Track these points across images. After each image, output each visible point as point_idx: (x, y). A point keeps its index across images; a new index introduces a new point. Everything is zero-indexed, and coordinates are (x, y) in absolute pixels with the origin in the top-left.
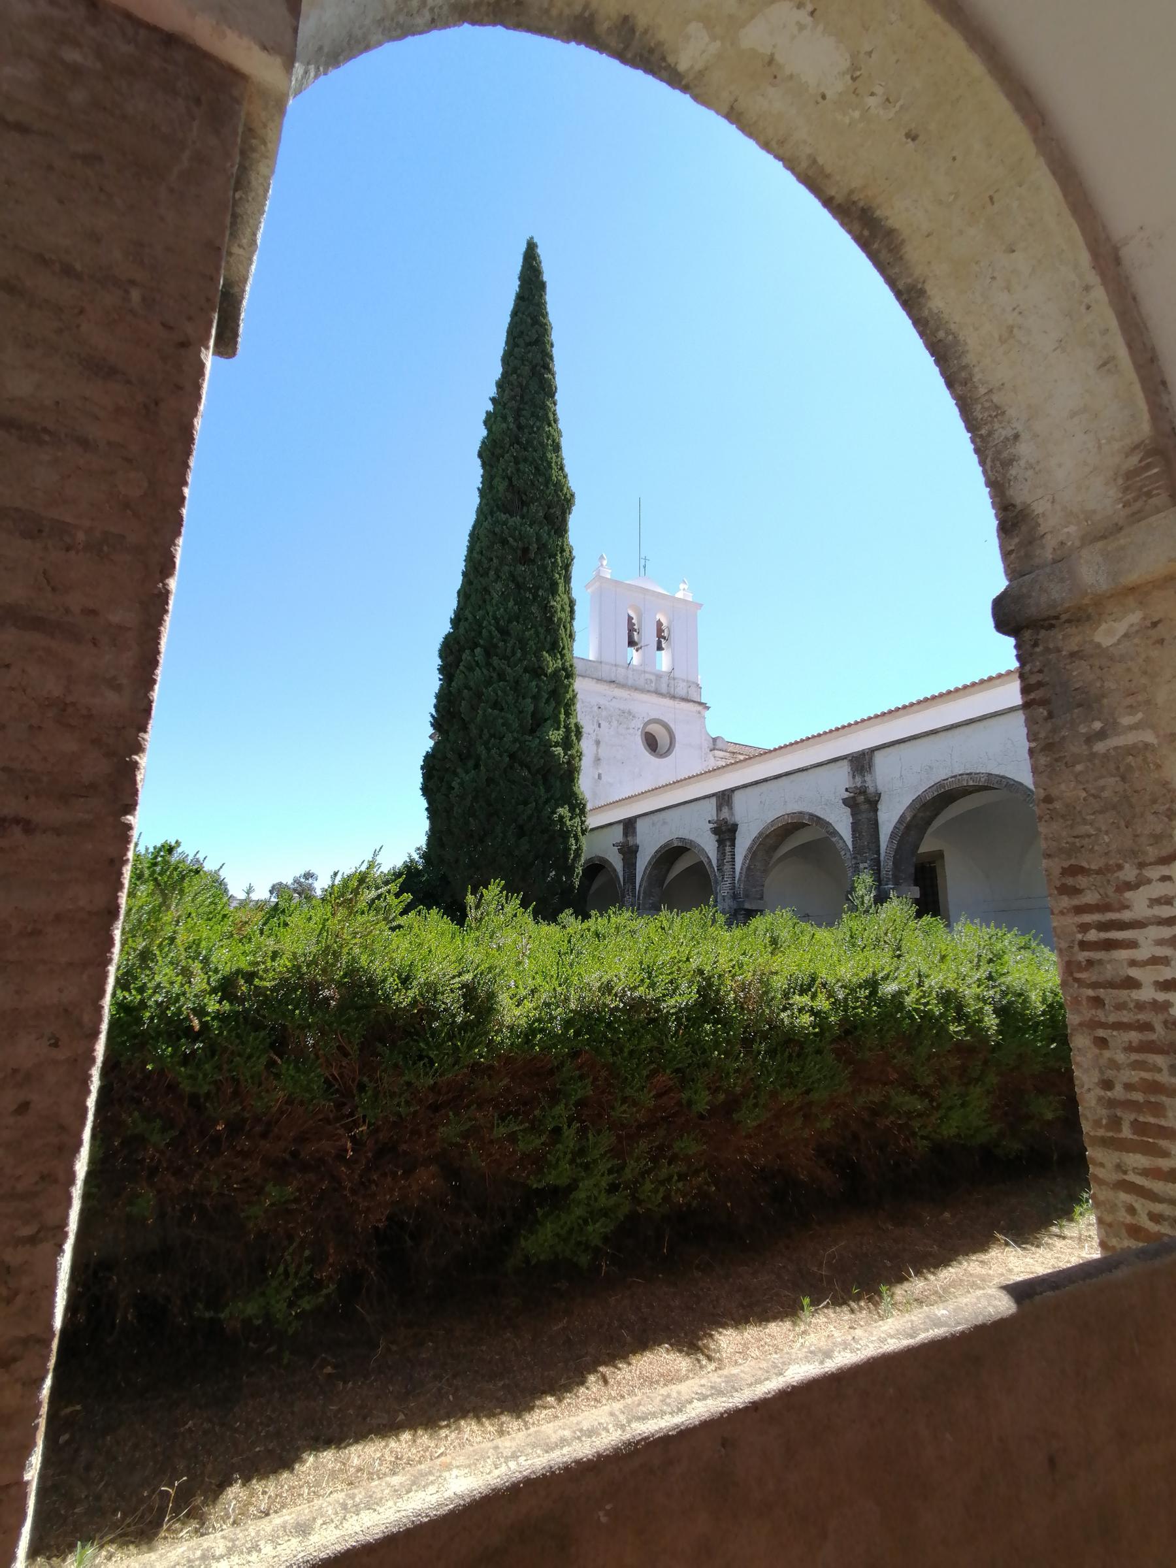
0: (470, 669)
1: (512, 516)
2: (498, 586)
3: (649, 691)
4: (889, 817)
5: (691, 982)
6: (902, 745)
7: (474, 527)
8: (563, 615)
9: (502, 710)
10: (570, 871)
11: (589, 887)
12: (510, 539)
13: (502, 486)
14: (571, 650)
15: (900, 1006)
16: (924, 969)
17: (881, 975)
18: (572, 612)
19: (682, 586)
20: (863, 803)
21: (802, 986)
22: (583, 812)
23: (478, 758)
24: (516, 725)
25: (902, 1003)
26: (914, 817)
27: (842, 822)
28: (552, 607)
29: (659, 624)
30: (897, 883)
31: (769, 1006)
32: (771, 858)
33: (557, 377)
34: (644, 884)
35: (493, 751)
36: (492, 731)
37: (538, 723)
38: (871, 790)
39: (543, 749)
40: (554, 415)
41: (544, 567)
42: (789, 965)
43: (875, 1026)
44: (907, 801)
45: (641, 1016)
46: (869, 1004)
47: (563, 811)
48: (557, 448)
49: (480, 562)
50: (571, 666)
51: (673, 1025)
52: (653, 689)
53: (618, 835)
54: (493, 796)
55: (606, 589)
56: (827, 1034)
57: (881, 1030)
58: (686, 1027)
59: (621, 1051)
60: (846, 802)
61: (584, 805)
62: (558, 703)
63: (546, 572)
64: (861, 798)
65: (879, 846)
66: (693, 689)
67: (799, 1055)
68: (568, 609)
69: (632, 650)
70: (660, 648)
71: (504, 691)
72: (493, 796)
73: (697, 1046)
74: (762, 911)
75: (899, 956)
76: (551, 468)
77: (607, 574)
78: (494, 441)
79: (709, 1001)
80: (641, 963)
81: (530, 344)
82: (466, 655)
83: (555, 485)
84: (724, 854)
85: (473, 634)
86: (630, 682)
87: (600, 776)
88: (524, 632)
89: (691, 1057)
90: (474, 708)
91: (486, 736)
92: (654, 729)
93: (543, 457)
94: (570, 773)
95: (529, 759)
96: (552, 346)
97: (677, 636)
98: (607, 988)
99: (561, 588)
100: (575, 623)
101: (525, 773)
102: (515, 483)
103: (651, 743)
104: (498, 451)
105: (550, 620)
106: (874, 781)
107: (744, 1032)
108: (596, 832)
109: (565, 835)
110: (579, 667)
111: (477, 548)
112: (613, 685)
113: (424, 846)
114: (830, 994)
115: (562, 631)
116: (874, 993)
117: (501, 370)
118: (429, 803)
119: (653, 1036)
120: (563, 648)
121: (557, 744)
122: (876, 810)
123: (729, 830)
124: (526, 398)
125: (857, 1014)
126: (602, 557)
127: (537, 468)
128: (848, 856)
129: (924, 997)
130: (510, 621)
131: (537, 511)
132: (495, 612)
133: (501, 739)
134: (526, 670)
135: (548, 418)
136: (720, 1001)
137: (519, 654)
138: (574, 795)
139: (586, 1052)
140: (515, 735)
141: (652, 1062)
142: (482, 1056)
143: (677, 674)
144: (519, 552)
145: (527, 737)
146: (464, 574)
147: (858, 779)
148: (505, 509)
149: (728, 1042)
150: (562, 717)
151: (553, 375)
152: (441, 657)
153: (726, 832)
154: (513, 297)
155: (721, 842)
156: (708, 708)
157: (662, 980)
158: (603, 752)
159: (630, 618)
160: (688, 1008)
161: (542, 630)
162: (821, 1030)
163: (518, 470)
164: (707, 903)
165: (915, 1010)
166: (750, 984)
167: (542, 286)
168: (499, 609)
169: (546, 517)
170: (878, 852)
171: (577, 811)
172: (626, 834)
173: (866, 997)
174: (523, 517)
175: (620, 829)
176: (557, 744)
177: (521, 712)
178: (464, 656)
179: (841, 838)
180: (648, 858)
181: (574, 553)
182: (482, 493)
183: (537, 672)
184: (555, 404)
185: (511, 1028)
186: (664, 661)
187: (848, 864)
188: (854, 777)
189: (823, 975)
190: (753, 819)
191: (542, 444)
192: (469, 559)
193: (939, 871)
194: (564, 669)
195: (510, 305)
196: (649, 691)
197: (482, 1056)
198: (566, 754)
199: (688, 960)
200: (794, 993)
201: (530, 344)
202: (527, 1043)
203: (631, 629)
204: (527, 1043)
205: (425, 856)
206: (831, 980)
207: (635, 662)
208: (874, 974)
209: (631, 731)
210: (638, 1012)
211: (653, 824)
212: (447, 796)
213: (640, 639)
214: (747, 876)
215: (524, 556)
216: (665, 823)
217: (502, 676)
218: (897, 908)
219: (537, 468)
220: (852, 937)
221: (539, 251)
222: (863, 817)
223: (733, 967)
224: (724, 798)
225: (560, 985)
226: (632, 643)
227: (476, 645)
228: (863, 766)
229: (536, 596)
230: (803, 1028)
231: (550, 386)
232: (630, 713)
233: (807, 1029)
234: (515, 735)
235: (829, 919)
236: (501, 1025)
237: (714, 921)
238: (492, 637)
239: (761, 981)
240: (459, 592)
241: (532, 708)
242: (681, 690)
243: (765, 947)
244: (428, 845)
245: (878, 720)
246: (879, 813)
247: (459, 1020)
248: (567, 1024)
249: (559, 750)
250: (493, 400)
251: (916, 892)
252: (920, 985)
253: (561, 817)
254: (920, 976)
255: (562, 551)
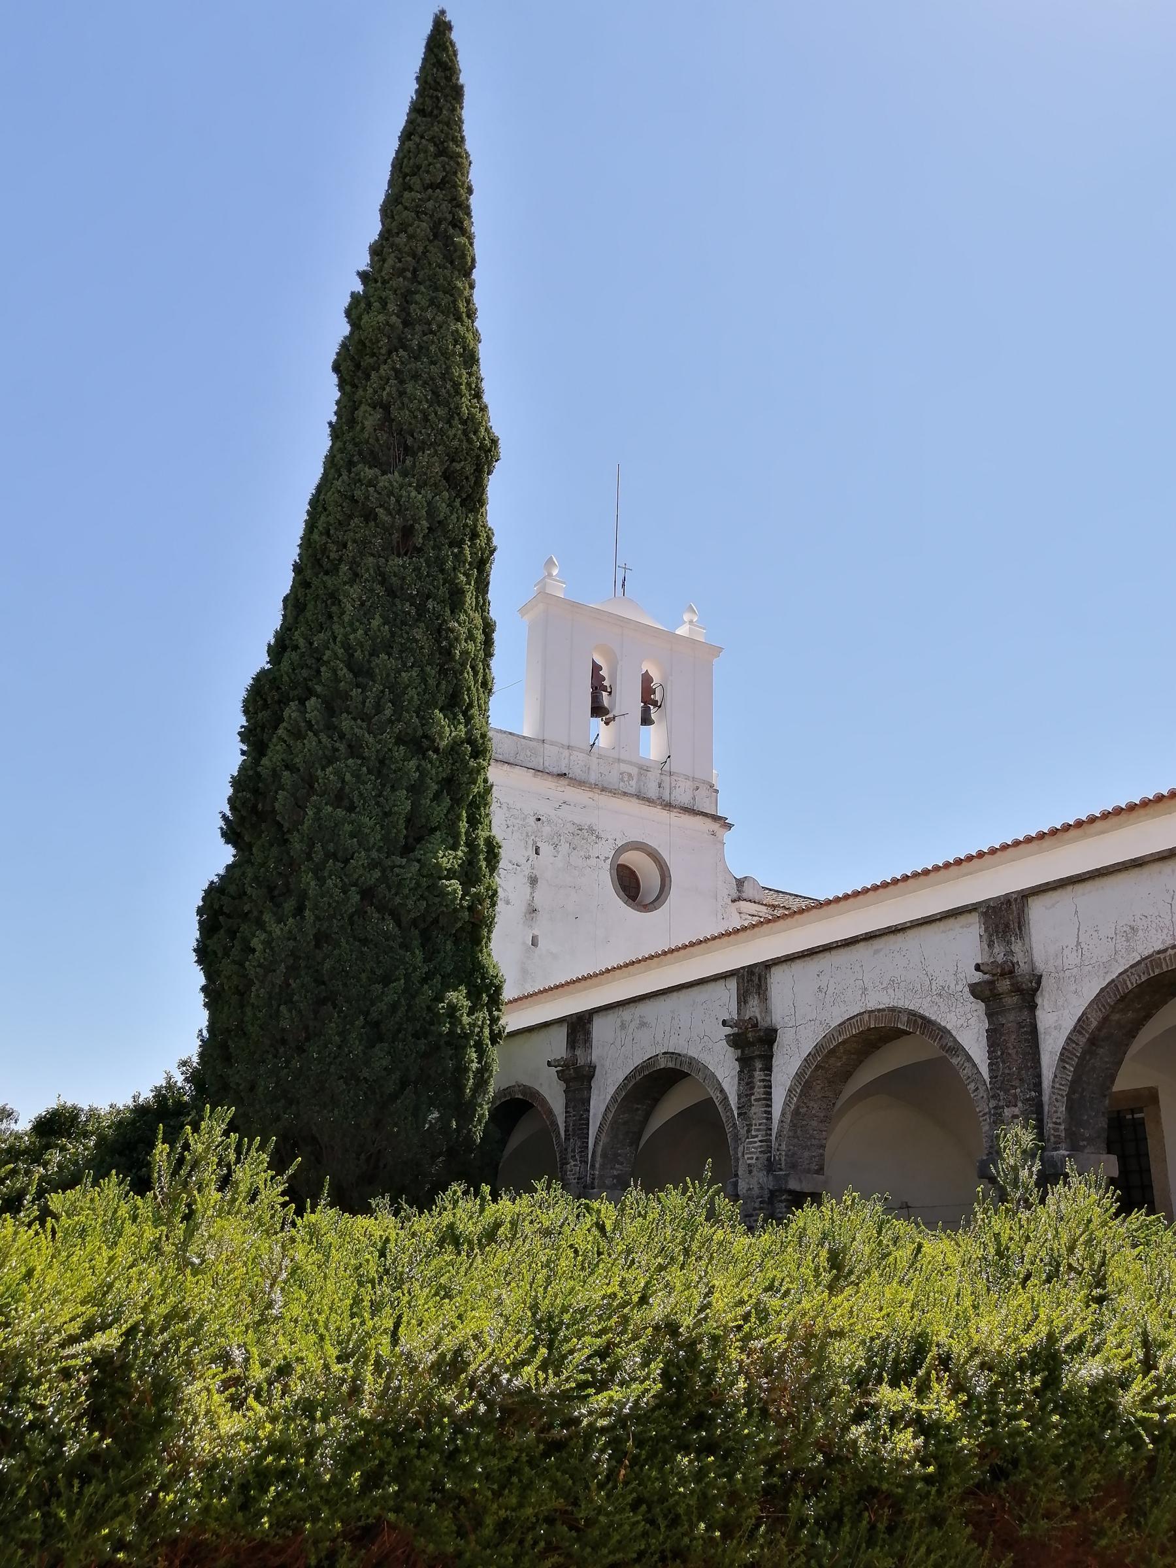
0: (298, 735)
1: (384, 473)
2: (355, 591)
3: (625, 794)
4: (1058, 1020)
5: (648, 1355)
6: (1079, 888)
7: (319, 488)
8: (471, 646)
9: (351, 809)
10: (465, 1111)
11: (503, 1142)
12: (380, 511)
13: (370, 419)
14: (484, 711)
15: (1110, 1414)
16: (1155, 1329)
17: (1068, 1339)
18: (488, 642)
19: (686, 617)
20: (1009, 993)
21: (896, 1361)
22: (495, 1001)
23: (303, 895)
24: (376, 838)
25: (1112, 1406)
26: (1105, 1020)
27: (969, 1029)
28: (452, 630)
29: (647, 679)
30: (1075, 1148)
31: (825, 1407)
32: (838, 1094)
33: (476, 241)
34: (604, 1138)
35: (330, 883)
36: (331, 847)
37: (418, 834)
38: (1023, 968)
39: (425, 882)
40: (468, 301)
41: (440, 563)
42: (869, 1314)
43: (1057, 1459)
44: (1091, 989)
45: (526, 1431)
46: (1042, 1408)
47: (458, 997)
48: (471, 359)
49: (324, 549)
50: (483, 736)
51: (601, 1458)
52: (632, 791)
53: (557, 1045)
54: (327, 965)
55: (555, 616)
56: (954, 1479)
57: (1071, 1467)
58: (635, 1461)
59: (479, 1523)
60: (976, 991)
61: (498, 989)
62: (457, 802)
63: (442, 571)
64: (1004, 985)
65: (1039, 1076)
66: (703, 792)
67: (890, 1530)
68: (480, 637)
69: (598, 723)
70: (646, 720)
71: (357, 776)
72: (327, 965)
73: (653, 1506)
74: (817, 1199)
75: (1100, 1300)
76: (458, 392)
77: (559, 591)
78: (361, 342)
79: (688, 1396)
80: (534, 1308)
81: (432, 186)
82: (291, 711)
83: (464, 423)
84: (750, 1085)
85: (305, 673)
86: (593, 778)
87: (535, 942)
88: (399, 671)
89: (645, 1534)
90: (300, 806)
91: (318, 856)
92: (633, 859)
93: (446, 375)
94: (474, 927)
95: (398, 900)
96: (470, 191)
97: (675, 697)
98: (451, 1367)
99: (470, 600)
100: (493, 663)
101: (390, 926)
102: (394, 413)
103: (628, 884)
104: (368, 360)
105: (448, 653)
106: (1029, 952)
107: (770, 1473)
108: (518, 1040)
109: (458, 1042)
110: (498, 746)
111: (321, 524)
112: (563, 782)
113: (195, 1059)
114: (958, 1388)
115: (468, 675)
116: (1052, 1381)
117: (379, 227)
118: (208, 976)
119: (555, 1484)
120: (470, 705)
121: (451, 874)
122: (1033, 1007)
123: (761, 1041)
124: (421, 275)
125: (1019, 1432)
126: (550, 563)
127: (435, 393)
128: (982, 1092)
129: (1157, 1392)
130: (374, 653)
131: (430, 465)
132: (346, 635)
133: (346, 861)
134: (399, 741)
135: (457, 309)
136: (715, 1399)
137: (388, 712)
138: (478, 968)
139: (393, 1527)
140: (374, 854)
141: (551, 1549)
142: (120, 1545)
143: (675, 766)
144: (396, 536)
145: (398, 860)
146: (297, 569)
147: (999, 949)
148: (373, 460)
149: (733, 1497)
150: (463, 826)
151: (470, 238)
152: (246, 712)
153: (754, 1043)
154: (405, 108)
155: (745, 1062)
156: (729, 826)
157: (581, 1350)
158: (542, 898)
159: (596, 668)
160: (640, 1416)
161: (431, 671)
162: (940, 1467)
163: (402, 394)
164: (697, 1176)
165: (1142, 1422)
166: (783, 1355)
167: (457, 93)
168: (355, 631)
169: (447, 476)
170: (1038, 1086)
171: (485, 998)
172: (572, 1043)
173: (1036, 1392)
174: (404, 474)
175: (562, 1033)
176: (451, 874)
177: (386, 814)
178: (286, 714)
179: (969, 1058)
180: (612, 1090)
181: (495, 541)
182: (336, 431)
183: (420, 744)
184: (472, 287)
185: (209, 1468)
186: (652, 743)
187: (983, 1107)
188: (991, 945)
189: (941, 1335)
190: (805, 1017)
191: (446, 355)
192: (307, 543)
193: (1150, 1128)
194: (470, 741)
195: (399, 120)
196: (625, 794)
197: (120, 1545)
198: (466, 893)
199: (644, 1300)
200: (879, 1380)
201: (432, 186)
202: (244, 1507)
203: (598, 686)
204: (244, 1507)
205: (195, 1078)
206: (959, 1350)
207: (602, 743)
208: (1051, 1336)
209: (593, 861)
210: (521, 1425)
211: (623, 1026)
212: (241, 964)
213: (613, 703)
214: (794, 1125)
215: (405, 541)
216: (643, 1025)
217: (354, 750)
218: (1083, 1199)
219: (435, 393)
220: (999, 1253)
221: (454, 36)
222: (1009, 1020)
223: (746, 1317)
224: (752, 980)
225: (339, 1360)
226: (598, 710)
227: (310, 692)
228: (1007, 926)
229: (421, 610)
230: (900, 1463)
231: (463, 256)
232: (591, 830)
233: (910, 1465)
234: (374, 854)
235: (950, 1217)
236: (183, 1459)
237: (711, 1215)
238: (337, 680)
239: (806, 1352)
240: (286, 600)
241: (408, 806)
242: (682, 796)
243: (817, 1274)
244: (201, 1055)
245: (1033, 846)
246: (1039, 1013)
247: (71, 1449)
248: (351, 1455)
249: (454, 885)
250: (364, 276)
251: (1110, 1165)
252: (1148, 1365)
253: (453, 1009)
254: (1146, 1344)
255: (475, 535)
